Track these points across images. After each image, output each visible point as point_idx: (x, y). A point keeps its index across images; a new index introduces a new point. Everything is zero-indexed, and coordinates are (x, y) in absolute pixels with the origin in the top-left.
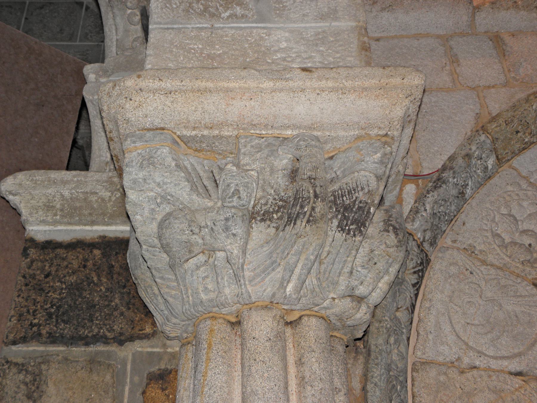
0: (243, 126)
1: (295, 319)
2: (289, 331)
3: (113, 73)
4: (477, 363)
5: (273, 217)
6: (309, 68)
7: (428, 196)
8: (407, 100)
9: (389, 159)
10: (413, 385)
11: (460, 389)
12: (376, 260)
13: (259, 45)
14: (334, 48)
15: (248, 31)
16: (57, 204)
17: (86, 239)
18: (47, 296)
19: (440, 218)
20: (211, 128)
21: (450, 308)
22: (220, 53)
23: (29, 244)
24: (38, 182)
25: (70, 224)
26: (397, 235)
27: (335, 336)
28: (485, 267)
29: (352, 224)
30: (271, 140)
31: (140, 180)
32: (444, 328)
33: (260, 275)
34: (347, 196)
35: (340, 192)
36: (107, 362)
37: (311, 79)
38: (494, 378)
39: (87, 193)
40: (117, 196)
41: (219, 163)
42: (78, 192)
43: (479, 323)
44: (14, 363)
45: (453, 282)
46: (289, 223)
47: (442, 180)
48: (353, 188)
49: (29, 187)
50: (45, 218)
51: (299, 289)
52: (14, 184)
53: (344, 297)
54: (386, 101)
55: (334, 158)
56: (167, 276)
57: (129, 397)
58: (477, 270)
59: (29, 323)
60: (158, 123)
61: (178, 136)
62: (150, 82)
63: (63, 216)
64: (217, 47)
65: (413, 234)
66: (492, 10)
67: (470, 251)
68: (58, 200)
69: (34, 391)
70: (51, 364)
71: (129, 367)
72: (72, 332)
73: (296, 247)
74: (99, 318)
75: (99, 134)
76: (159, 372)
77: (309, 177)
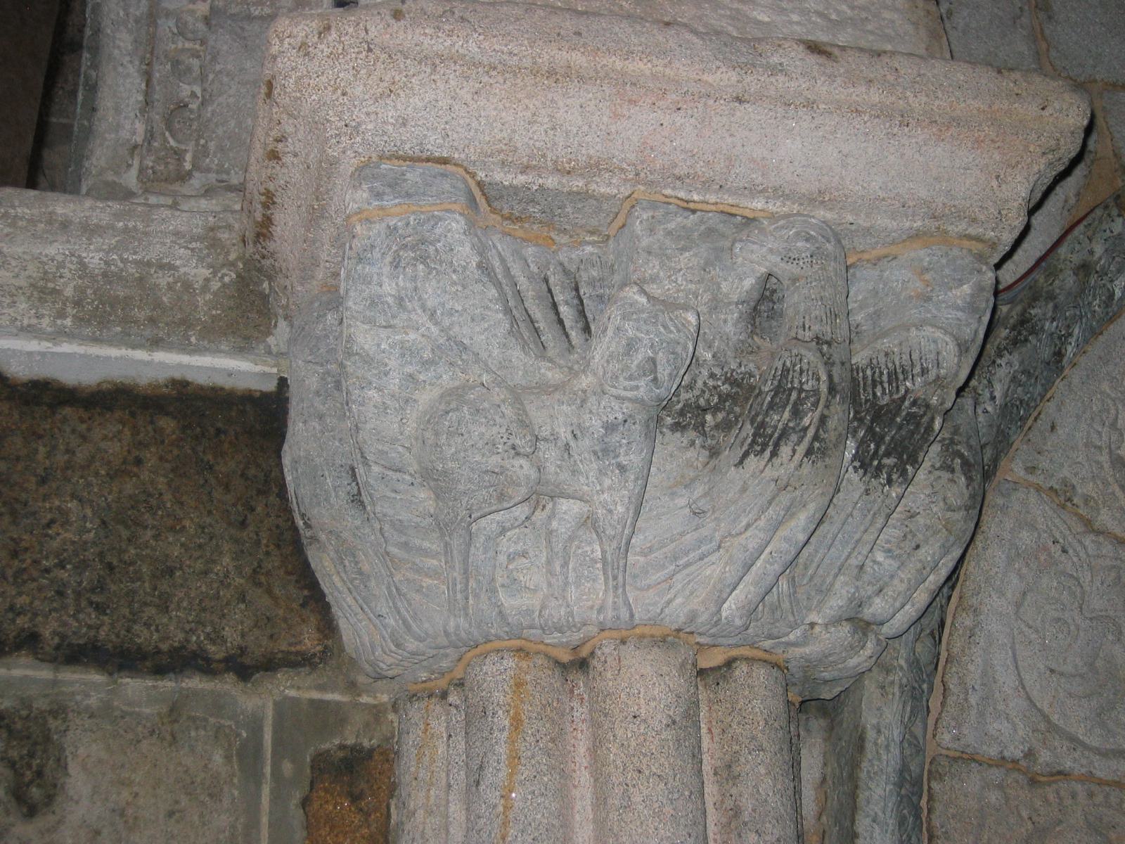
0: (650, 177)
4: (1068, 764)
6: (825, 44)
7: (999, 361)
11: (1029, 823)
16: (65, 285)
17: (137, 385)
18: (47, 535)
20: (569, 173)
21: (1016, 632)
24: (20, 223)
25: (96, 340)
30: (714, 220)
31: (390, 300)
32: (1002, 680)
33: (663, 567)
34: (886, 385)
35: (869, 372)
36: (212, 720)
37: (832, 77)
38: (1099, 799)
39: (149, 264)
40: (227, 279)
41: (562, 257)
42: (123, 260)
45: (1024, 570)
47: (1029, 325)
48: (902, 366)
50: (34, 321)
56: (417, 542)
57: (271, 812)
58: (1076, 544)
60: (434, 144)
61: (480, 184)
62: (425, 34)
63: (82, 320)
67: (1063, 496)
68: (68, 275)
69: (31, 782)
70: (70, 715)
72: (118, 636)
74: (185, 604)
75: (120, 69)
76: (341, 754)
77: (817, 338)
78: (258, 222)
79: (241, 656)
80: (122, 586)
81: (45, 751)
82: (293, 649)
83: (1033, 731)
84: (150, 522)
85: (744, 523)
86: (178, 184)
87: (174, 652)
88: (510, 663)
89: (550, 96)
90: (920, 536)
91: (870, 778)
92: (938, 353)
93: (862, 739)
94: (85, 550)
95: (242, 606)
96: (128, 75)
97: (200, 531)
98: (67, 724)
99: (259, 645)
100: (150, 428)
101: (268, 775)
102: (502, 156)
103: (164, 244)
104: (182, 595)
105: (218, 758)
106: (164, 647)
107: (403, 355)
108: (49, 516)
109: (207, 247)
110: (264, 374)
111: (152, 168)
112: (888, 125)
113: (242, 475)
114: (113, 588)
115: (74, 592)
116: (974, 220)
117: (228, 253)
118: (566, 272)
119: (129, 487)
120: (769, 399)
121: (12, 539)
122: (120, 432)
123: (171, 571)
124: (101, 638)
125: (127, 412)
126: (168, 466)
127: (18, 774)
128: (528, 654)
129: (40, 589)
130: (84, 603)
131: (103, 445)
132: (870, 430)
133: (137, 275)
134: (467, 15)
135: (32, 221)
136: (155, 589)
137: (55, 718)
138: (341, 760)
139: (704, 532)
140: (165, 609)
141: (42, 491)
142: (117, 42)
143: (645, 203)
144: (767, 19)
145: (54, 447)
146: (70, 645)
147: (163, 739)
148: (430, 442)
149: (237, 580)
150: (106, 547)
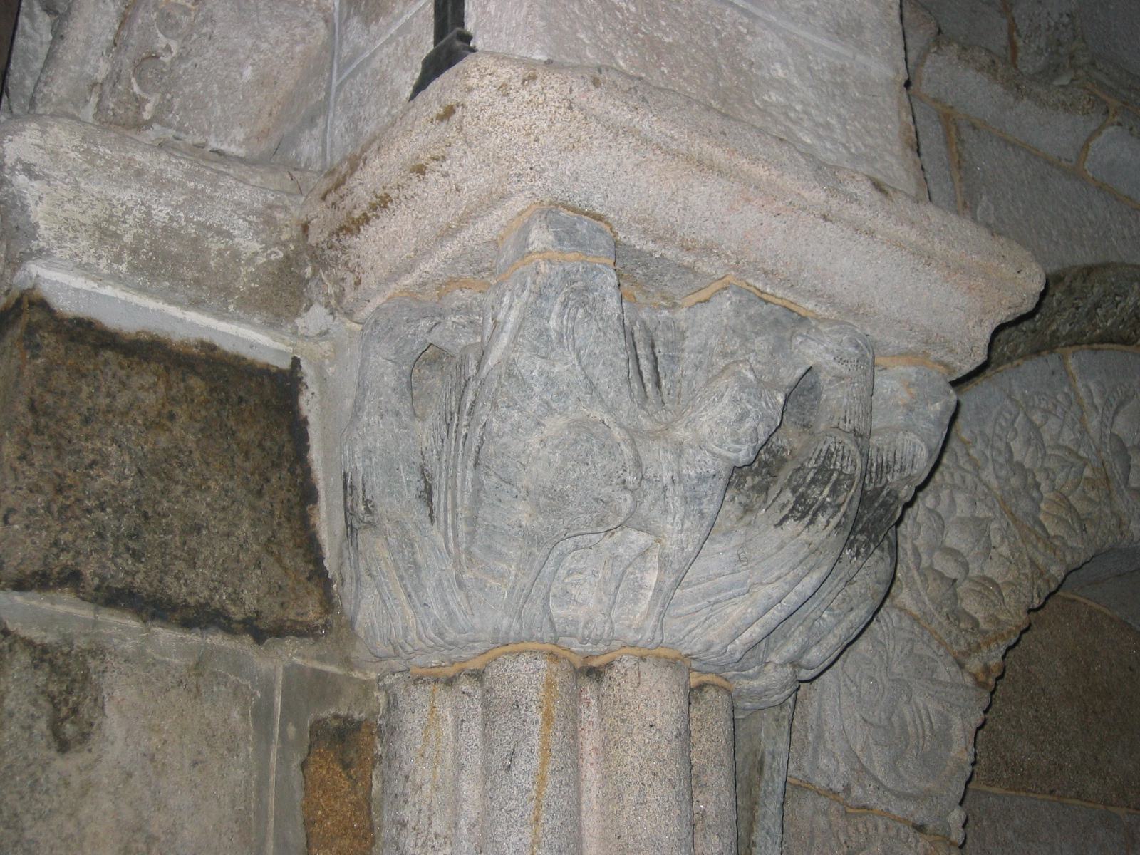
4: (872, 801)
16: (127, 231)
17: (170, 341)
18: (89, 475)
24: (98, 162)
25: (141, 290)
29: (861, 532)
33: (696, 601)
34: (873, 475)
36: (232, 677)
38: (893, 832)
39: (210, 228)
40: (273, 257)
42: (188, 220)
44: (23, 639)
48: (887, 462)
50: (93, 260)
56: (498, 547)
59: (52, 540)
63: (136, 268)
66: (956, 61)
69: (66, 718)
70: (108, 658)
71: (278, 700)
72: (151, 585)
74: (210, 562)
76: (335, 723)
78: (353, 219)
79: (256, 619)
80: (156, 536)
81: (82, 689)
82: (300, 619)
84: (181, 477)
85: (776, 574)
86: (133, 131)
88: (542, 664)
90: (855, 601)
93: (761, 763)
94: (124, 496)
95: (259, 572)
96: (107, 13)
98: (105, 665)
99: (272, 612)
100: (182, 385)
102: (645, 225)
103: (225, 211)
104: (207, 553)
105: (236, 715)
106: (192, 601)
107: (546, 384)
108: (92, 457)
109: (262, 223)
110: (279, 352)
111: (113, 109)
113: (260, 445)
114: (148, 537)
115: (113, 535)
116: (951, 351)
117: (280, 232)
118: (646, 330)
119: (163, 440)
120: (811, 474)
122: (155, 384)
123: (198, 529)
124: (137, 585)
126: (197, 425)
127: (56, 708)
128: (557, 659)
129: (83, 528)
130: (122, 549)
131: (141, 394)
133: (194, 236)
134: (647, 96)
135: (110, 163)
136: (184, 543)
137: (93, 657)
139: (737, 576)
143: (735, 289)
144: (809, 141)
145: (98, 389)
146: (108, 587)
147: (190, 690)
148: (556, 465)
150: (143, 496)
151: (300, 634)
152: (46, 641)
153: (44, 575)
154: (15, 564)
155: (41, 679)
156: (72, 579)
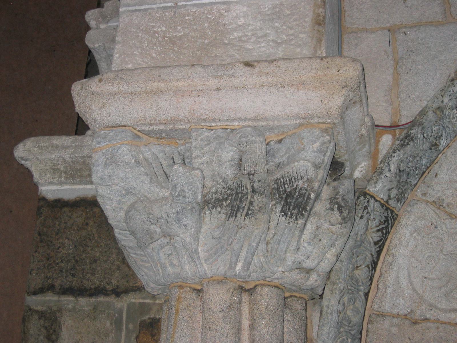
1: (251, 287)
2: (245, 297)
3: (111, 18)
4: (428, 316)
5: (223, 204)
6: (251, 61)
7: (393, 155)
8: (344, 90)
9: (327, 148)
10: (367, 336)
12: (320, 237)
13: (218, 23)
14: (288, 24)
15: (208, 7)
17: (88, 197)
19: (408, 174)
20: (166, 124)
22: (182, 35)
23: (42, 203)
24: (44, 148)
26: (341, 212)
27: (294, 296)
28: (450, 220)
29: (294, 209)
30: (220, 132)
31: (106, 177)
36: (107, 311)
38: (441, 329)
39: (84, 157)
41: (179, 149)
42: (76, 157)
43: (436, 277)
44: (35, 310)
46: (232, 215)
47: (410, 138)
49: (36, 153)
50: (52, 180)
51: (248, 264)
52: (25, 150)
53: (292, 270)
54: (324, 92)
55: (282, 142)
60: (119, 121)
61: (139, 131)
62: (110, 86)
63: (67, 178)
64: (179, 28)
65: (375, 196)
67: (438, 204)
68: (61, 163)
72: (78, 284)
73: (238, 236)
74: (100, 272)
76: (149, 321)
79: (117, 289)
82: (134, 285)
83: (413, 303)
84: (90, 245)
87: (96, 288)
89: (154, 99)
91: (323, 326)
92: (306, 170)
97: (106, 246)
100: (91, 212)
101: (124, 329)
105: (108, 324)
106: (93, 287)
108: (59, 245)
112: (277, 88)
119: (84, 233)
121: (47, 254)
122: (82, 214)
123: (96, 261)
125: (84, 207)
126: (97, 225)
132: (286, 200)
133: (82, 161)
134: (123, 76)
135: (47, 147)
138: (149, 323)
140: (93, 274)
141: (57, 237)
142: (102, 66)
146: (64, 288)
149: (117, 262)
151: (134, 291)
152: (43, 310)
153: (42, 288)
154: (33, 287)
155: (42, 322)
156: (51, 288)
